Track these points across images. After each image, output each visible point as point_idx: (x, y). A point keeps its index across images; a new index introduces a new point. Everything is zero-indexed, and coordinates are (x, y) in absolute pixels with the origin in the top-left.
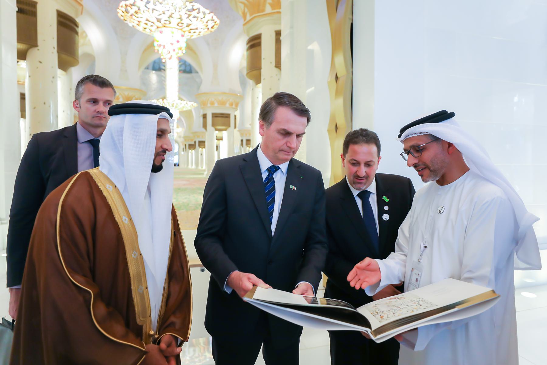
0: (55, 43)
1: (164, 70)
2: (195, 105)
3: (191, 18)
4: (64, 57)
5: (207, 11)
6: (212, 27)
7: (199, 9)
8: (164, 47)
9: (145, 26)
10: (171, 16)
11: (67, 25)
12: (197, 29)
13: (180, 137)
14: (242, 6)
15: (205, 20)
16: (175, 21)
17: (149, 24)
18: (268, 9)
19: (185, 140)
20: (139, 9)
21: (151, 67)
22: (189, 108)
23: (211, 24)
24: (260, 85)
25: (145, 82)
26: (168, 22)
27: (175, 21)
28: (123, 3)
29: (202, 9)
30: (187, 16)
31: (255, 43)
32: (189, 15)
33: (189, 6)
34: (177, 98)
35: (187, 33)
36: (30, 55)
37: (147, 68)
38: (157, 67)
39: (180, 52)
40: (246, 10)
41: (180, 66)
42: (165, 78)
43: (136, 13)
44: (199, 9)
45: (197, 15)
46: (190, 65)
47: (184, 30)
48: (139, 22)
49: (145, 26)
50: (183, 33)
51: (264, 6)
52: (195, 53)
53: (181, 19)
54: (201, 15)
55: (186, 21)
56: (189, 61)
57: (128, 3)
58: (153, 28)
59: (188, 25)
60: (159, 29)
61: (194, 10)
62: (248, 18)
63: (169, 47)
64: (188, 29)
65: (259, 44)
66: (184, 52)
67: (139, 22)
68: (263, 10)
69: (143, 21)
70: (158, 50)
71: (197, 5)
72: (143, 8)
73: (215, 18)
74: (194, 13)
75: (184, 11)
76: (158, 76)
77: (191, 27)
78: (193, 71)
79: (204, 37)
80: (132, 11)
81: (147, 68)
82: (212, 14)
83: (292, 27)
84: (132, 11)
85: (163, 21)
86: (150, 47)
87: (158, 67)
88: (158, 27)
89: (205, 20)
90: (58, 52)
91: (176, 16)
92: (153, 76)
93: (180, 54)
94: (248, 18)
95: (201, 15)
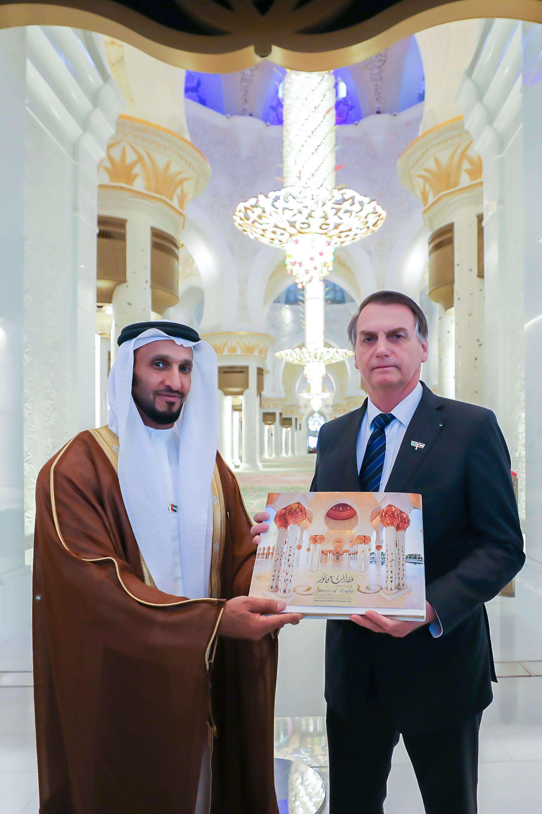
0: (147, 275)
1: (303, 302)
2: (351, 353)
3: (340, 214)
4: (160, 293)
5: (366, 200)
6: (374, 225)
7: (353, 198)
8: (300, 264)
9: (273, 236)
10: (310, 216)
11: (164, 245)
12: (350, 230)
13: (327, 406)
14: (420, 181)
15: (363, 214)
16: (316, 223)
17: (279, 231)
18: (465, 180)
19: (335, 411)
20: (264, 212)
21: (283, 299)
22: (341, 359)
23: (372, 219)
24: (452, 310)
25: (274, 322)
26: (306, 226)
27: (316, 223)
28: (241, 206)
29: (359, 198)
30: (334, 211)
31: (443, 240)
32: (338, 210)
33: (338, 196)
34: (322, 344)
35: (335, 239)
36: (116, 297)
37: (277, 301)
38: (292, 299)
39: (325, 269)
40: (428, 187)
41: (327, 293)
42: (303, 313)
43: (260, 217)
44: (353, 198)
45: (350, 208)
46: (342, 290)
47: (330, 234)
48: (264, 230)
49: (273, 236)
50: (329, 239)
51: (458, 176)
52: (348, 269)
53: (325, 217)
54: (356, 207)
55: (333, 220)
56: (341, 283)
57: (248, 204)
58: (284, 238)
59: (336, 227)
60: (294, 238)
61: (345, 200)
62: (431, 199)
63: (308, 265)
64: (336, 232)
65: (450, 241)
66: (331, 269)
67: (264, 230)
68: (456, 184)
69: (270, 228)
70: (292, 271)
71: (349, 193)
72: (269, 209)
73: (379, 209)
74: (346, 206)
75: (330, 204)
76: (294, 312)
77: (341, 228)
78: (347, 299)
79: (363, 242)
80: (253, 216)
81: (277, 301)
82: (374, 203)
83: (501, 202)
84: (253, 216)
85: (298, 225)
86: (280, 268)
87: (294, 297)
88: (291, 235)
89: (363, 214)
90: (152, 287)
91: (318, 213)
92: (287, 313)
93: (325, 273)
94: (431, 199)
95: (356, 207)
